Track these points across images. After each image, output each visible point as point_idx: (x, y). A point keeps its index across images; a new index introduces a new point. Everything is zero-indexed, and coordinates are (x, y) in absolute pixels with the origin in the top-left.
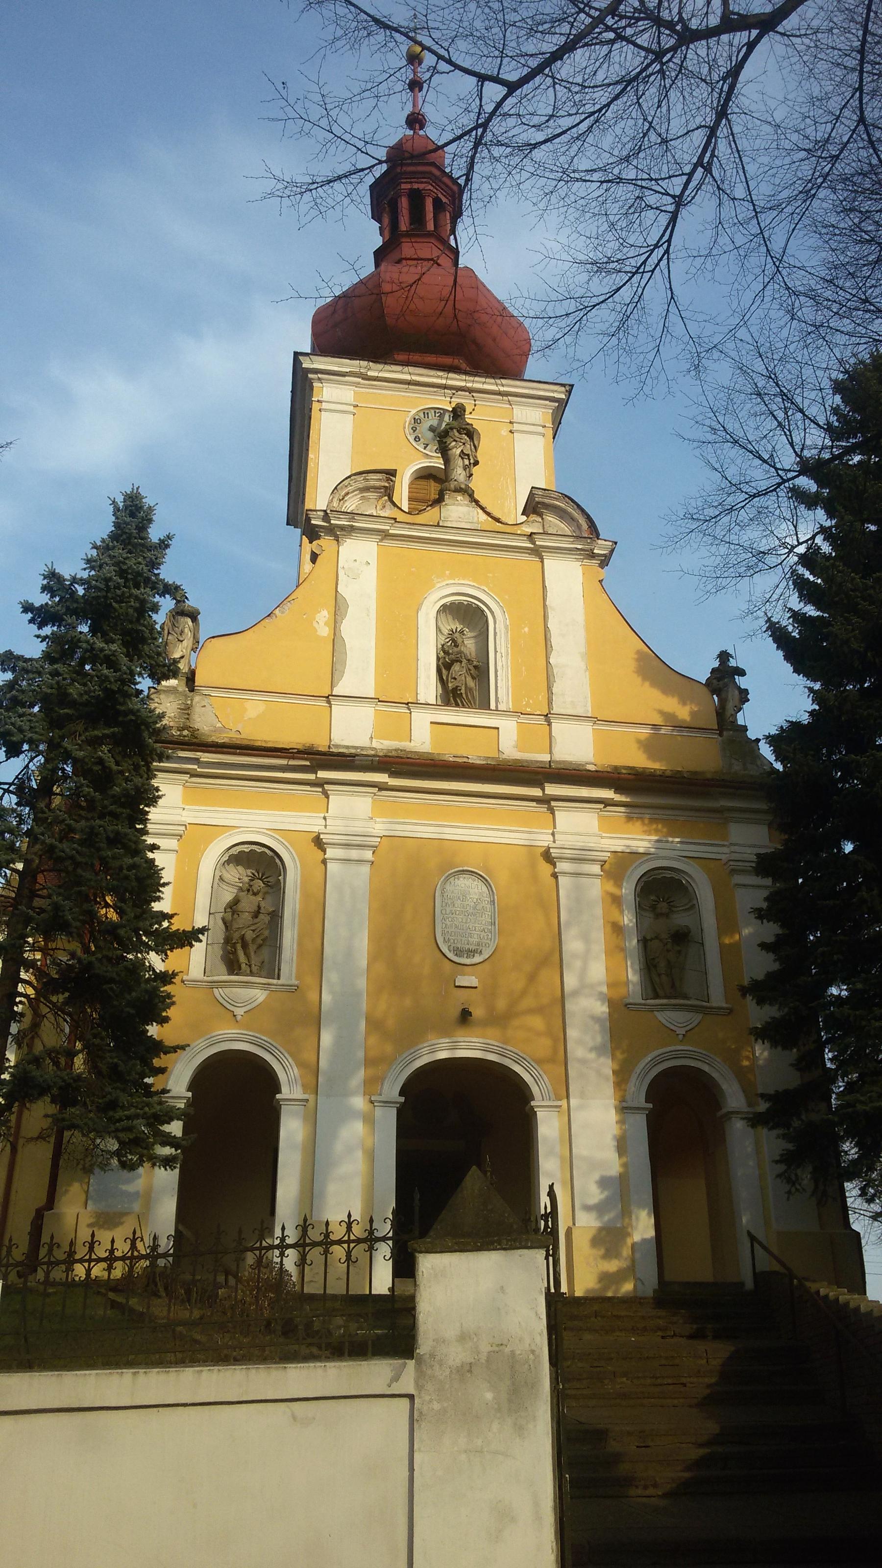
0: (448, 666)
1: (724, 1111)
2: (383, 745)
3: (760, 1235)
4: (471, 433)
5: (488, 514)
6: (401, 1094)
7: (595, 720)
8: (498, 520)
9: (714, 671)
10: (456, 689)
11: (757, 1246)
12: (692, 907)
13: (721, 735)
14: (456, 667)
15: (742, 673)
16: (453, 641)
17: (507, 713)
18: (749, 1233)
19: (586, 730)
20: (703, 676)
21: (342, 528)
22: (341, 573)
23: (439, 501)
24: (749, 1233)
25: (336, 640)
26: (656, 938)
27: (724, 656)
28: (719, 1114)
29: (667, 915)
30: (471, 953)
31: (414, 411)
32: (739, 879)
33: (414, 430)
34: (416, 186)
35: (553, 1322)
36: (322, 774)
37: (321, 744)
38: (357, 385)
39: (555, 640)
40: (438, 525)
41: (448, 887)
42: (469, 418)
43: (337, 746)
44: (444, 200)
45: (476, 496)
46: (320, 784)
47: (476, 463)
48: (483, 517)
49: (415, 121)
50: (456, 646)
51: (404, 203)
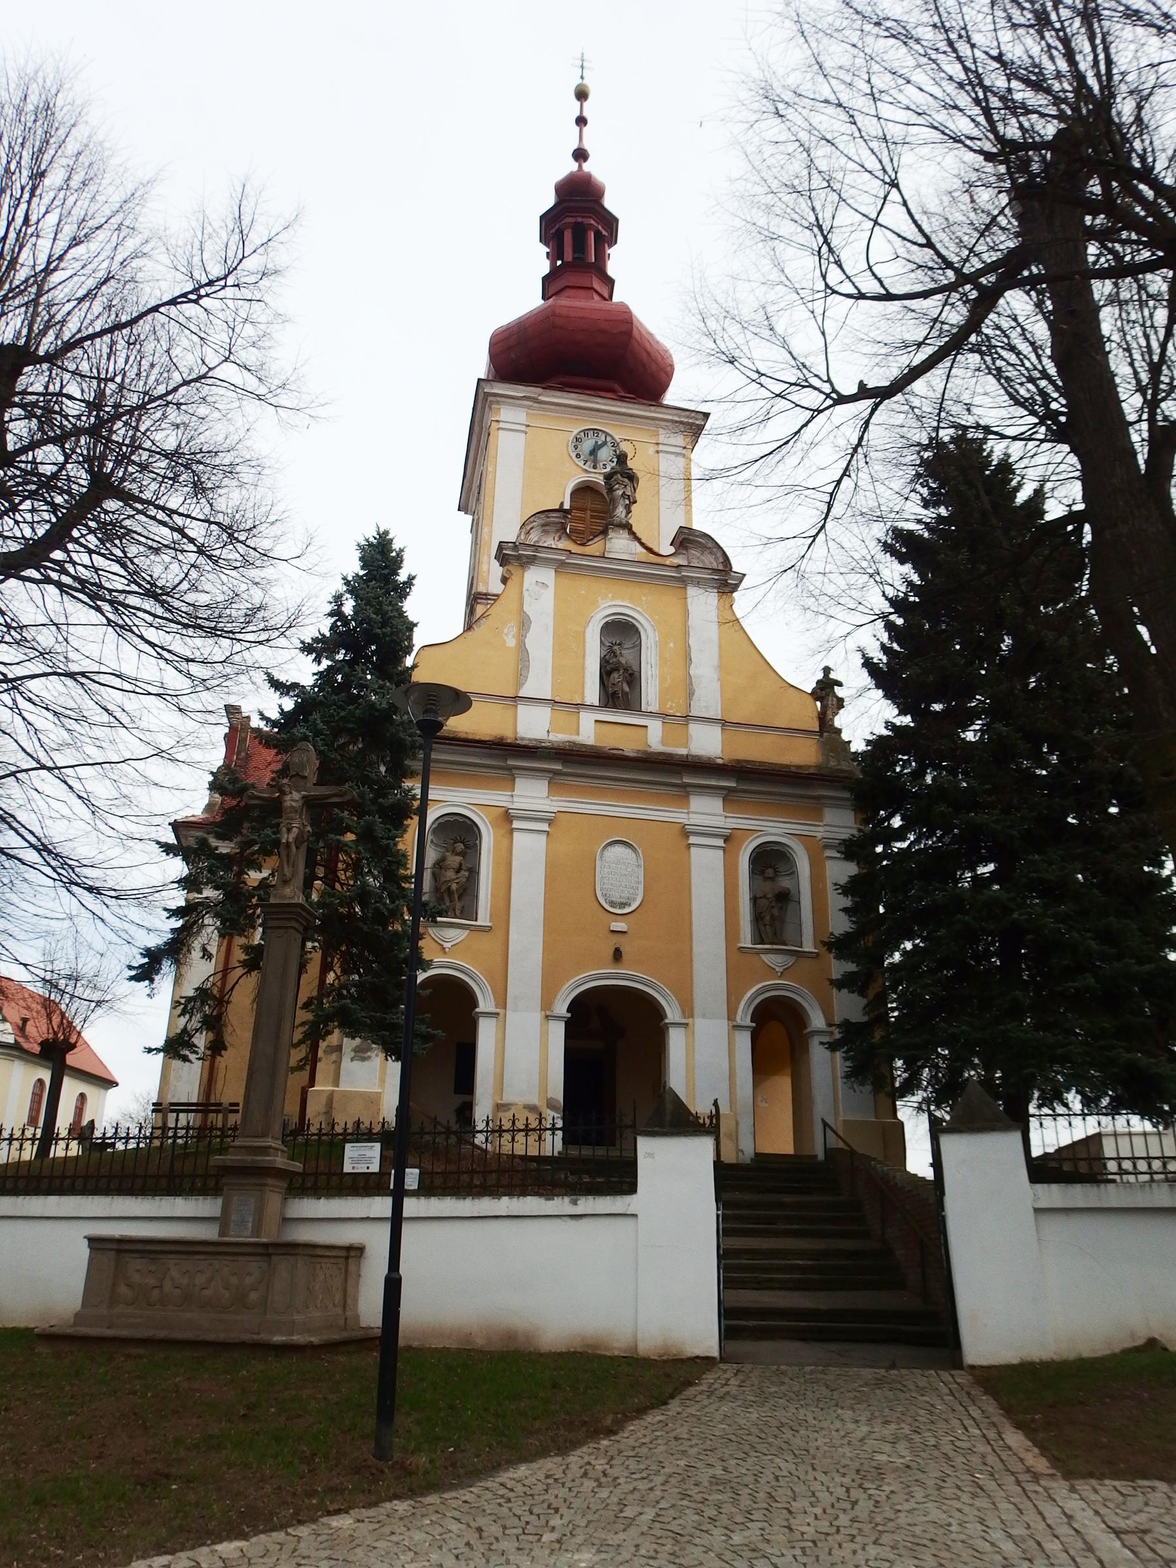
0: (609, 673)
1: (809, 1029)
2: (559, 737)
3: (830, 1121)
4: (632, 478)
5: (642, 544)
6: (568, 1011)
7: (724, 723)
8: (650, 550)
9: (818, 682)
10: (615, 693)
11: (828, 1131)
12: (793, 873)
13: (821, 736)
14: (615, 675)
15: (840, 684)
16: (614, 652)
17: (651, 714)
18: (823, 1120)
19: (716, 731)
20: (809, 687)
21: (527, 556)
22: (526, 594)
23: (604, 533)
24: (823, 1120)
25: (522, 648)
26: (764, 897)
27: (827, 670)
28: (805, 1032)
29: (772, 879)
30: (623, 905)
31: (576, 432)
32: (829, 853)
33: (576, 447)
34: (580, 220)
35: (164, 1183)
36: (510, 762)
37: (509, 735)
38: (529, 407)
39: (694, 655)
40: (604, 557)
41: (606, 853)
42: (630, 464)
43: (523, 739)
44: (604, 233)
45: (634, 529)
46: (510, 769)
47: (635, 502)
48: (640, 549)
49: (580, 155)
50: (616, 656)
51: (568, 236)
